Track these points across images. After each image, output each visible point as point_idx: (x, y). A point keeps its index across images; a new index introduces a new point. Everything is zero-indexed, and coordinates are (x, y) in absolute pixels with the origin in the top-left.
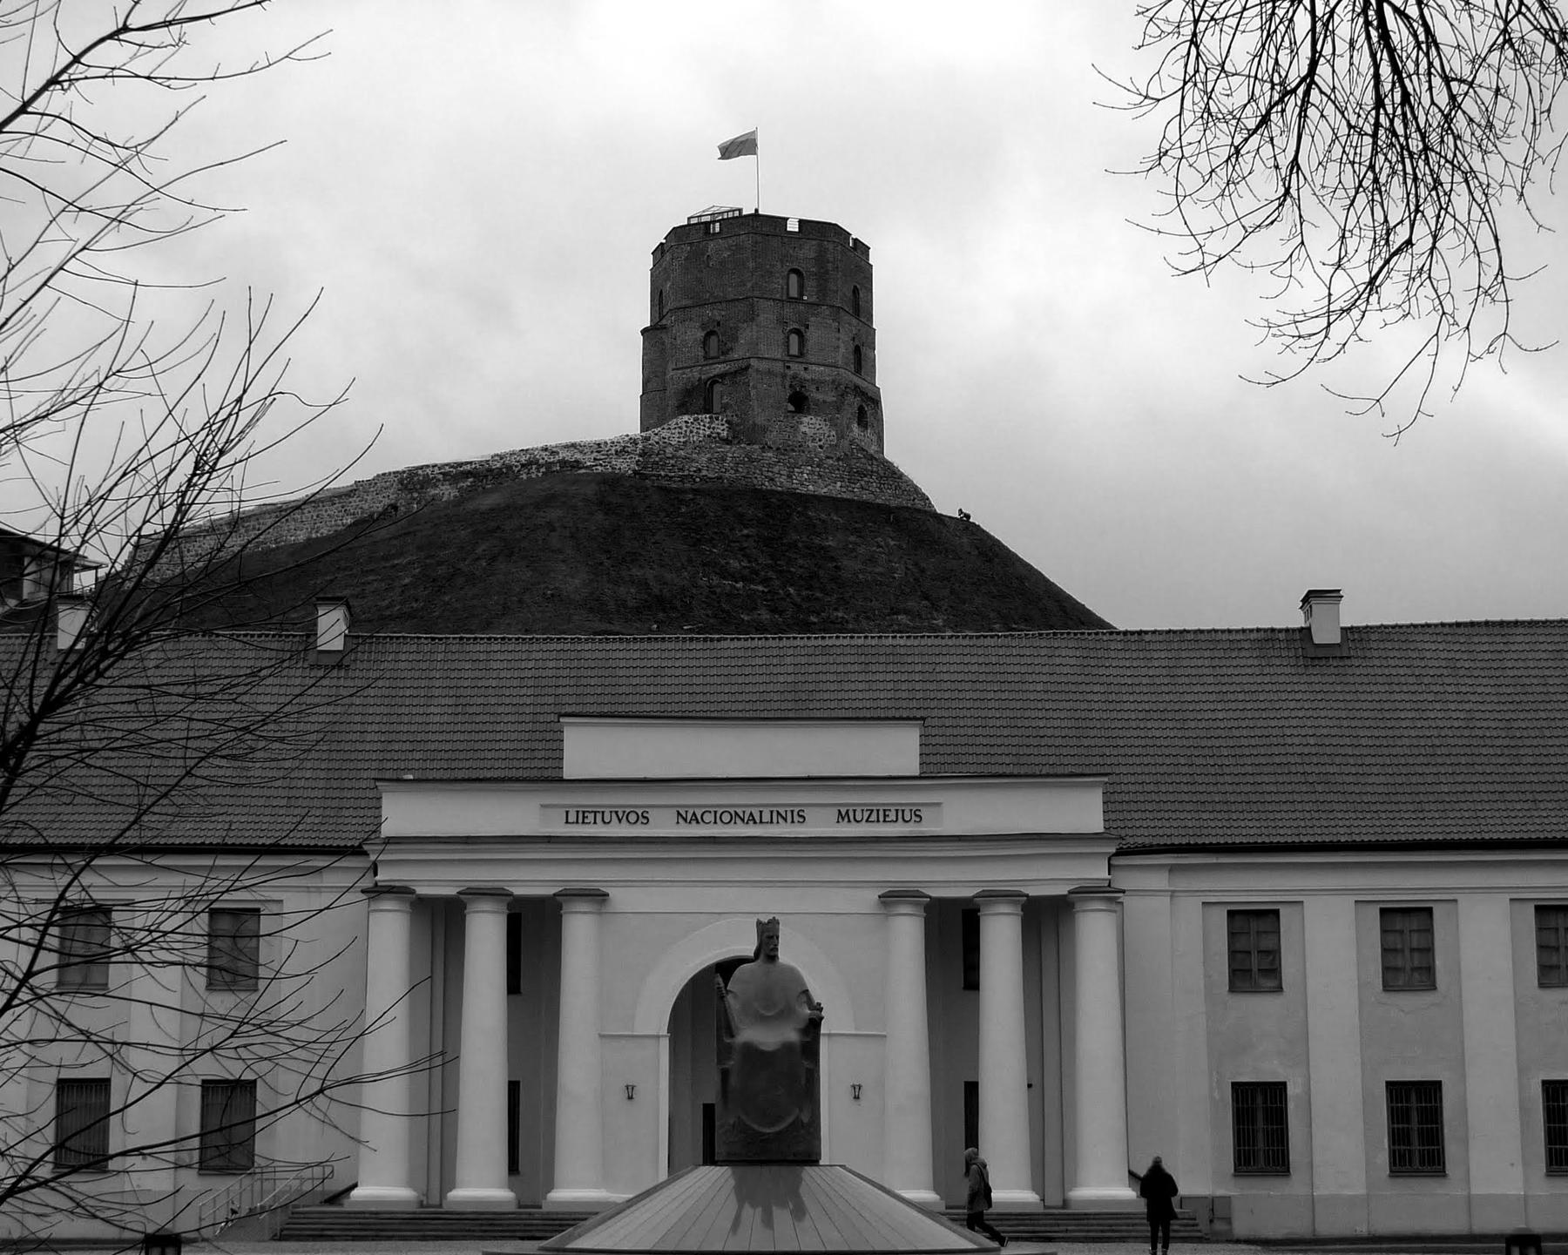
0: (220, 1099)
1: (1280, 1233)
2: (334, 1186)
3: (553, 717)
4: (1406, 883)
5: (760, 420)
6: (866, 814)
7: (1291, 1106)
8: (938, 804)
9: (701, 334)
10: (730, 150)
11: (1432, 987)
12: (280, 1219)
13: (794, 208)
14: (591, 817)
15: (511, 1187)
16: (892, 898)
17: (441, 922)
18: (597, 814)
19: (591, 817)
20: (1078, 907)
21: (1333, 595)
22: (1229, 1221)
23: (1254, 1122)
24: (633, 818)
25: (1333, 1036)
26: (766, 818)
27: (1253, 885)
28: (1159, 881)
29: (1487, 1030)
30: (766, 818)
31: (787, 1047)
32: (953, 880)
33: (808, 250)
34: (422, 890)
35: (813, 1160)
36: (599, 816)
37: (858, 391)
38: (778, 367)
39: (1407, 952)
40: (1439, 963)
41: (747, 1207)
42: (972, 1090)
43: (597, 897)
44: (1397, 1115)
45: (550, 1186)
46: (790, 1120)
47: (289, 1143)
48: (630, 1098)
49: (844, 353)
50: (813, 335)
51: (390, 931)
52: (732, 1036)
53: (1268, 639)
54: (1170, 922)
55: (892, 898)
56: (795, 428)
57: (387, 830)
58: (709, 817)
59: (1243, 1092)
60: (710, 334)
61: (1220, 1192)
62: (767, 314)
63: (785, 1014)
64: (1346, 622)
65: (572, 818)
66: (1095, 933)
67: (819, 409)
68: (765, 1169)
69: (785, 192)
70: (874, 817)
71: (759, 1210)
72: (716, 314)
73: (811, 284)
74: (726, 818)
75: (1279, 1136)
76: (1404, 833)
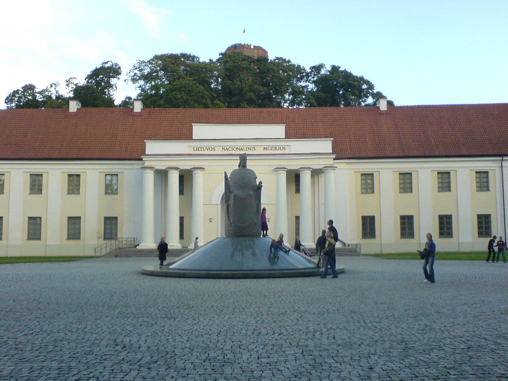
0: (108, 222)
2: (136, 243)
15: (180, 243)
17: (162, 175)
32: (293, 165)
34: (157, 168)
40: (452, 185)
42: (297, 218)
43: (202, 169)
44: (364, 224)
47: (125, 232)
74: (235, 149)
75: (411, 229)
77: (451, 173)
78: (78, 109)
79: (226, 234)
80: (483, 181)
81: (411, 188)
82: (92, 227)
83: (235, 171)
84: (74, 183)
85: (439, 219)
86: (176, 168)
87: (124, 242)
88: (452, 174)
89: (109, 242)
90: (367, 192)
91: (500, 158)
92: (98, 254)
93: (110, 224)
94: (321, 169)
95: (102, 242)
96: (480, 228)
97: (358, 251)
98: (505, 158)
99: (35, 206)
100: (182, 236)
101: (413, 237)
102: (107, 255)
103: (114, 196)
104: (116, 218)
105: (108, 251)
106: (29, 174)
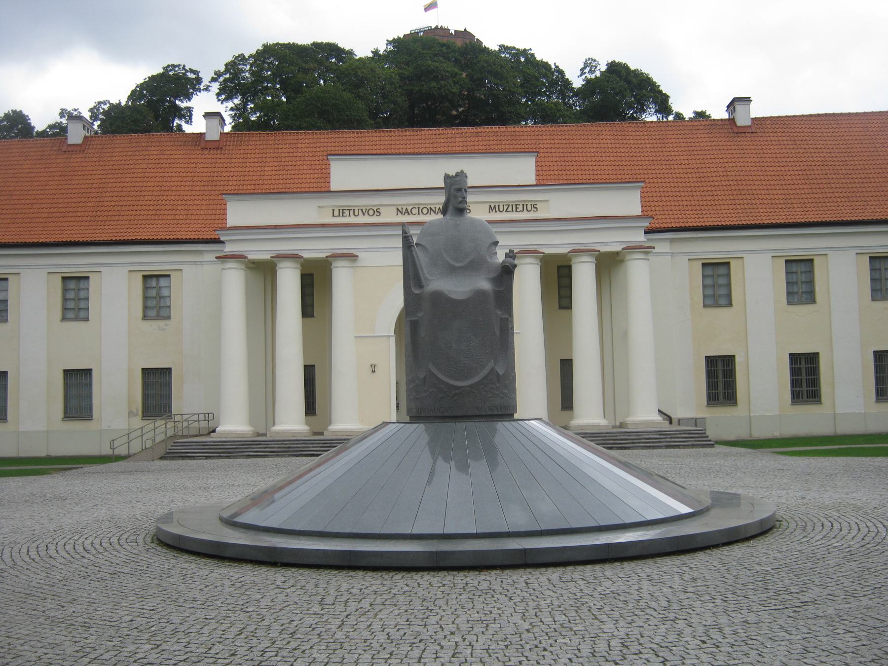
1: (732, 437)
3: (325, 158)
4: (799, 245)
6: (506, 208)
7: (737, 368)
8: (547, 201)
10: (428, 8)
11: (813, 301)
13: (454, 26)
14: (347, 213)
15: (307, 424)
17: (264, 272)
18: (351, 211)
19: (347, 213)
20: (628, 257)
21: (747, 100)
24: (371, 212)
25: (762, 331)
27: (716, 248)
29: (843, 324)
31: (480, 294)
34: (251, 257)
36: (352, 212)
39: (800, 283)
40: (817, 289)
41: (440, 462)
42: (567, 366)
43: (351, 257)
44: (711, 375)
45: (330, 423)
47: (186, 400)
48: (374, 371)
51: (234, 279)
52: (421, 286)
57: (231, 221)
58: (415, 211)
59: (711, 361)
61: (698, 416)
63: (475, 265)
64: (753, 116)
65: (336, 213)
68: (460, 425)
70: (510, 209)
74: (425, 211)
77: (816, 262)
78: (86, 137)
81: (729, 296)
85: (876, 361)
88: (733, 265)
89: (149, 425)
90: (716, 305)
93: (156, 385)
94: (617, 253)
95: (137, 422)
96: (795, 383)
99: (803, 331)
100: (310, 408)
101: (819, 402)
103: (161, 323)
104: (168, 371)
106: (783, 261)
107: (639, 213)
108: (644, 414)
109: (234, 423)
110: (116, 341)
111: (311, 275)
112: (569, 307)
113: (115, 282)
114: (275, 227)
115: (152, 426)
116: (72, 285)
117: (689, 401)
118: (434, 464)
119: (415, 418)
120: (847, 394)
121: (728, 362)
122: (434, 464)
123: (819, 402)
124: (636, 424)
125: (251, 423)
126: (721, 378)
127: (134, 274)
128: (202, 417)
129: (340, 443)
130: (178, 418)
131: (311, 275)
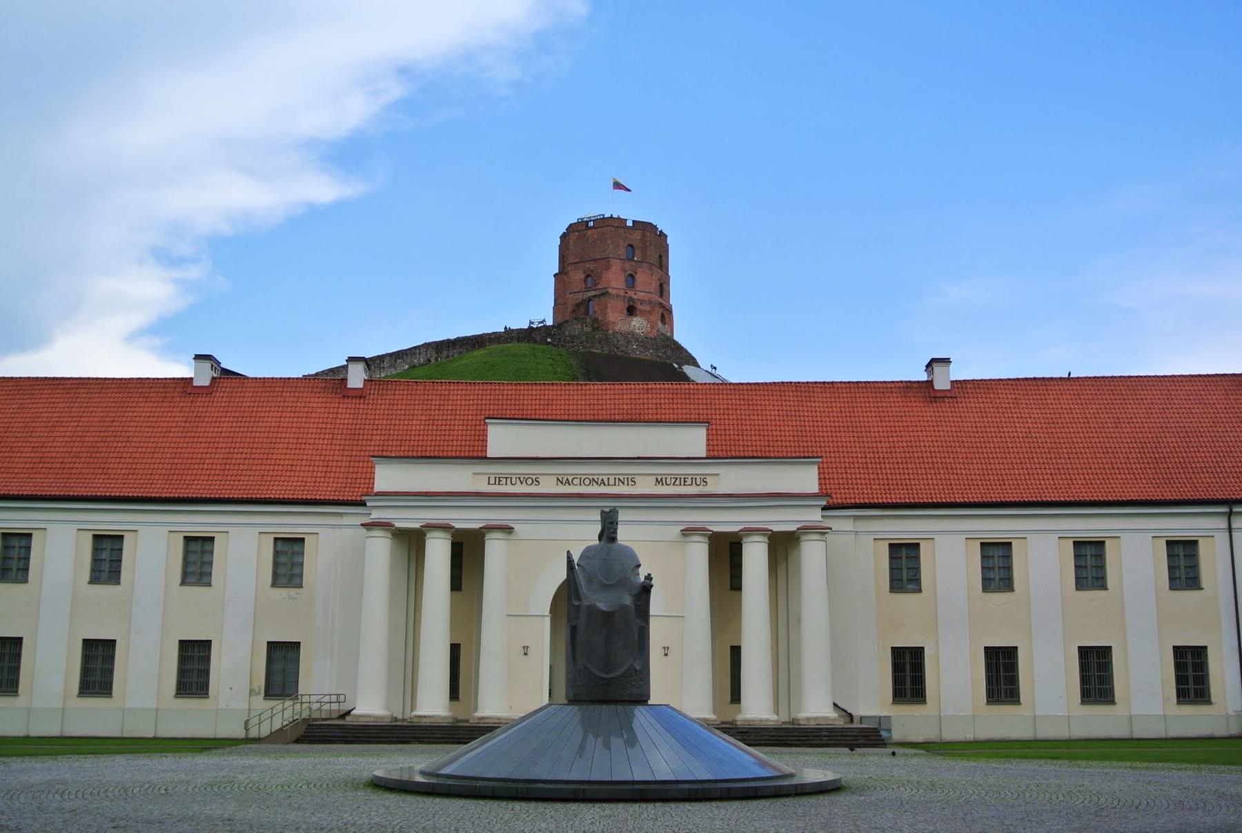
1: (920, 739)
2: (345, 707)
4: (996, 526)
5: (611, 319)
9: (583, 276)
12: (301, 730)
16: (688, 532)
17: (412, 543)
20: (803, 538)
21: (946, 361)
22: (889, 731)
23: (904, 671)
24: (529, 481)
25: (953, 621)
26: (612, 482)
27: (904, 528)
28: (847, 525)
30: (612, 482)
32: (726, 521)
33: (637, 235)
34: (398, 525)
35: (643, 699)
37: (661, 305)
38: (622, 293)
42: (736, 651)
43: (508, 530)
44: (898, 668)
45: (476, 709)
46: (626, 667)
47: (317, 683)
49: (654, 286)
50: (639, 278)
51: (380, 547)
52: (580, 600)
53: (908, 387)
54: (863, 542)
55: (688, 532)
56: (630, 324)
57: (379, 486)
59: (898, 653)
60: (588, 276)
62: (616, 266)
65: (492, 481)
66: (812, 553)
67: (643, 314)
69: (629, 210)
71: (600, 739)
72: (591, 266)
73: (638, 252)
74: (587, 482)
75: (1013, 680)
76: (995, 498)
78: (213, 378)
79: (567, 695)
80: (1183, 564)
82: (236, 668)
83: (588, 549)
84: (197, 559)
86: (445, 528)
87: (315, 706)
88: (924, 547)
89: (277, 704)
91: (1224, 509)
92: (254, 733)
93: (282, 659)
94: (793, 533)
95: (260, 703)
97: (884, 734)
98: (1236, 509)
100: (454, 693)
101: (1018, 702)
102: (277, 737)
104: (297, 645)
105: (277, 726)
107: (816, 490)
108: (816, 707)
109: (371, 705)
110: (239, 610)
111: (461, 544)
112: (739, 588)
113: (243, 543)
114: (427, 494)
115: (280, 707)
116: (195, 547)
117: (873, 699)
118: (584, 740)
119: (572, 701)
120: (1233, 698)
121: (916, 655)
122: (584, 740)
123: (1018, 702)
124: (808, 719)
125: (387, 708)
126: (909, 672)
127: (264, 536)
128: (334, 698)
129: (484, 729)
130: (305, 699)
131: (461, 544)
